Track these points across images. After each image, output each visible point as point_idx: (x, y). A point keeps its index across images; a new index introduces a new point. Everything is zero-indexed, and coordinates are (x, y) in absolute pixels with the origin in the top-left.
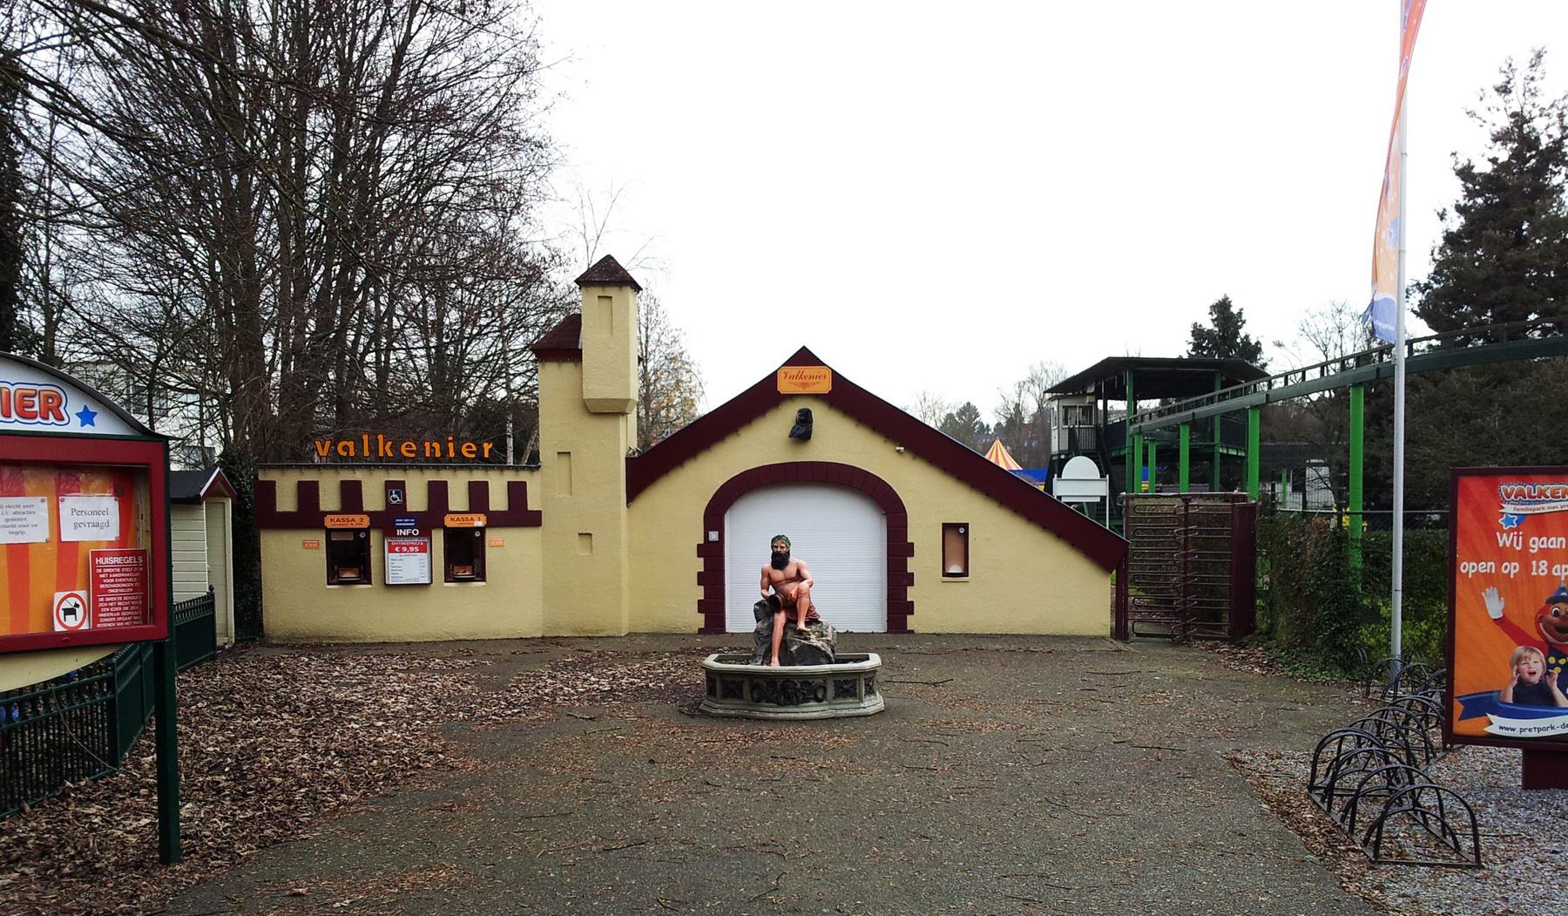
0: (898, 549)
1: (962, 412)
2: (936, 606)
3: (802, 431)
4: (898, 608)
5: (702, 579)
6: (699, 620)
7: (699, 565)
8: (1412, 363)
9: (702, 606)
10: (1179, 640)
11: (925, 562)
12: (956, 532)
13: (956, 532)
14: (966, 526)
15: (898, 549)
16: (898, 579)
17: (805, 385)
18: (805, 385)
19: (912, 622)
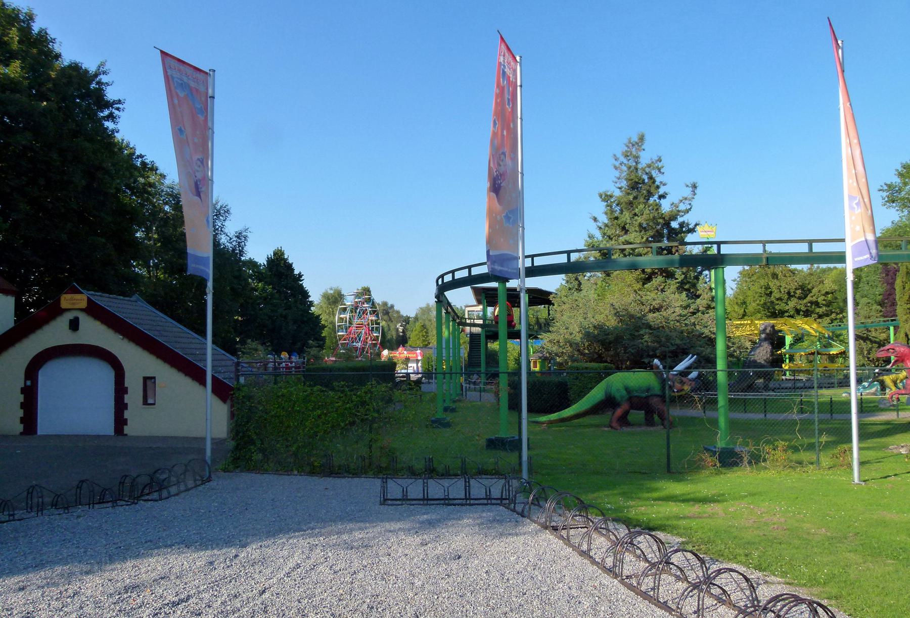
0: (120, 390)
1: (275, 254)
2: (140, 423)
3: (74, 325)
4: (120, 422)
5: (23, 406)
6: (20, 428)
7: (21, 398)
8: (857, 271)
9: (22, 420)
10: (202, 258)
11: (133, 397)
12: (148, 382)
13: (148, 382)
14: (154, 378)
15: (120, 390)
16: (120, 406)
17: (74, 304)
18: (74, 304)
19: (127, 430)
